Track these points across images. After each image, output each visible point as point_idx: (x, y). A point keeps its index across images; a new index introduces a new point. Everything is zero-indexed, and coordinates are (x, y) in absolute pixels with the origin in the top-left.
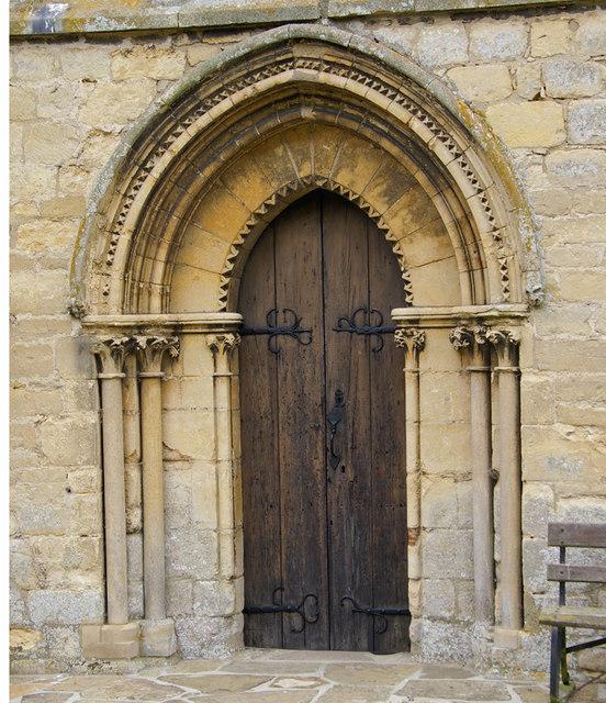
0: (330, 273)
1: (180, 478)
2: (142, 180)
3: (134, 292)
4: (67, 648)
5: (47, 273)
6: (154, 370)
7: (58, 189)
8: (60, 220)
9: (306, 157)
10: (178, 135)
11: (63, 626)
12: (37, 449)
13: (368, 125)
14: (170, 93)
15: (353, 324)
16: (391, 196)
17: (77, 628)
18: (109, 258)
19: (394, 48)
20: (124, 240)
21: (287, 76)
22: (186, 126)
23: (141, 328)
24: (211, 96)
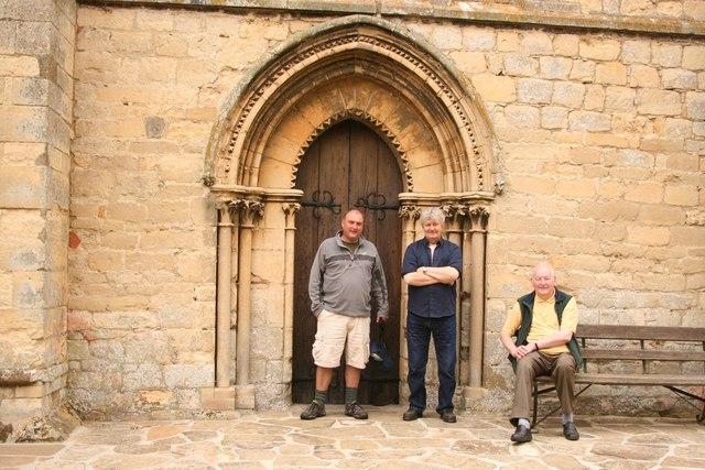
0: (354, 170)
1: (261, 294)
2: (256, 100)
3: (243, 172)
4: (191, 403)
5: (187, 155)
6: (249, 223)
7: (198, 102)
8: (199, 122)
9: (351, 97)
10: (281, 74)
11: (188, 388)
12: (174, 271)
13: (394, 80)
14: (280, 48)
15: (366, 203)
16: (402, 125)
17: (197, 390)
18: (231, 148)
19: (420, 34)
20: (241, 137)
21: (353, 45)
22: (286, 69)
23: (245, 195)
24: (304, 53)
